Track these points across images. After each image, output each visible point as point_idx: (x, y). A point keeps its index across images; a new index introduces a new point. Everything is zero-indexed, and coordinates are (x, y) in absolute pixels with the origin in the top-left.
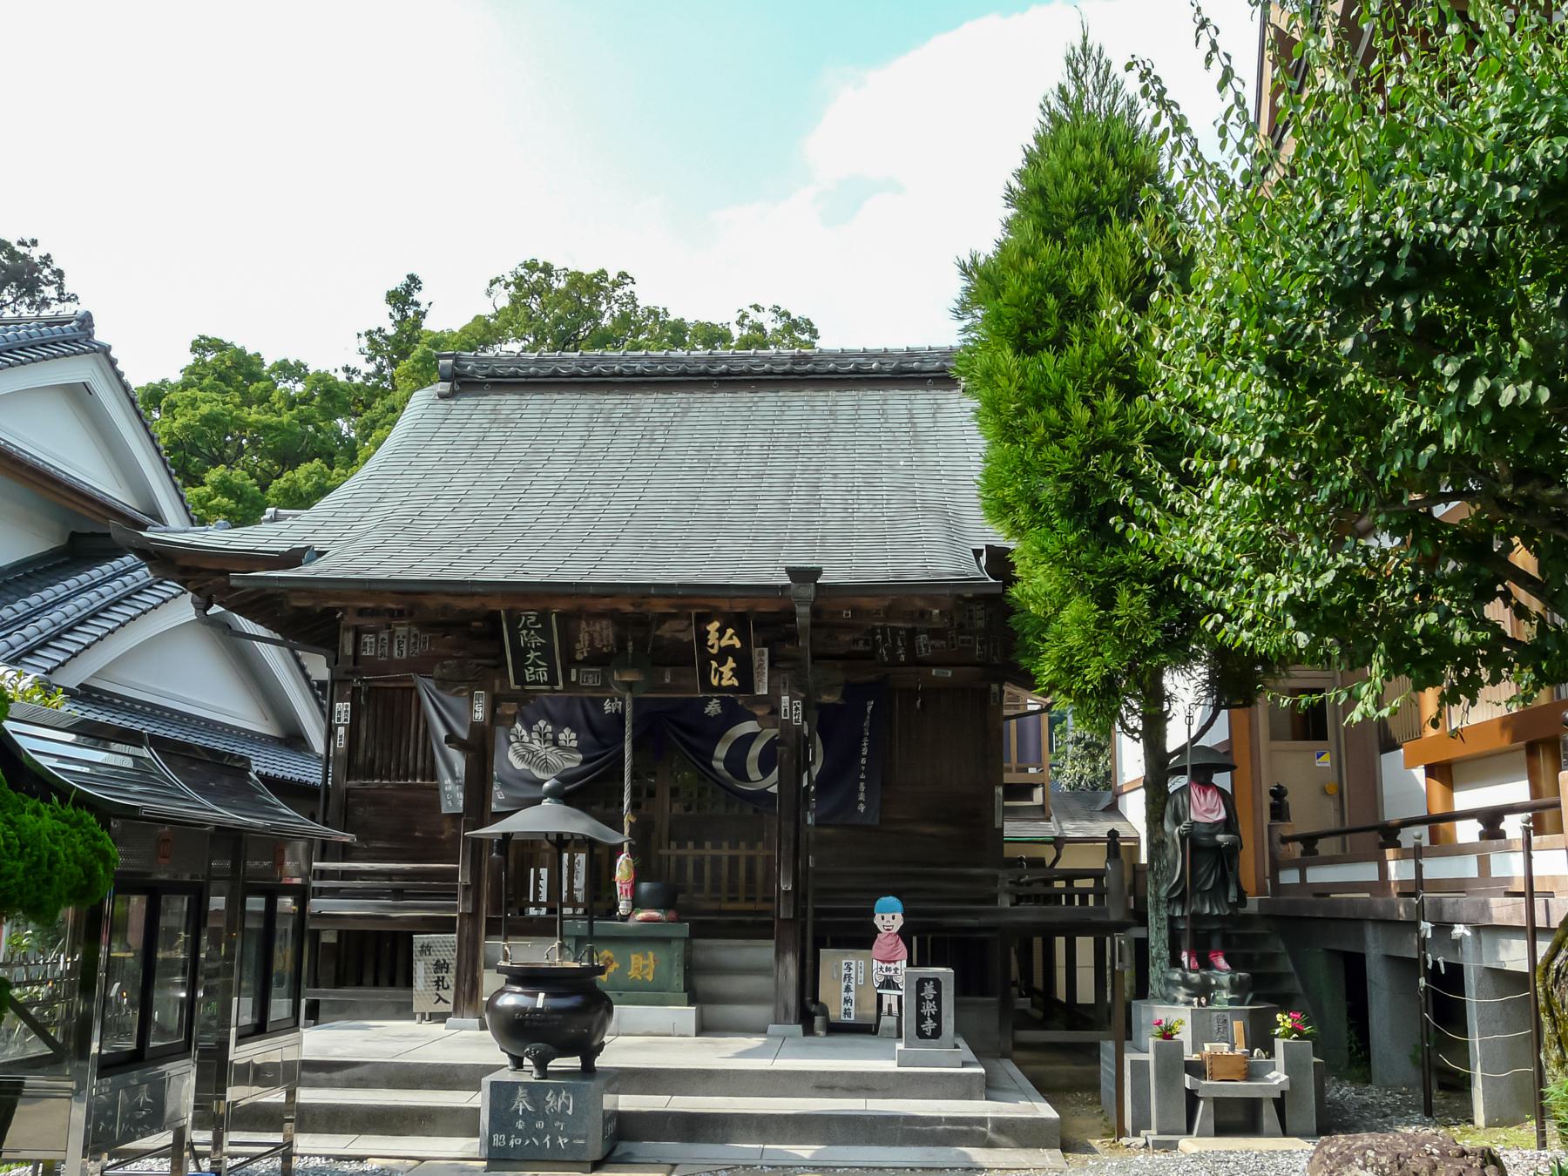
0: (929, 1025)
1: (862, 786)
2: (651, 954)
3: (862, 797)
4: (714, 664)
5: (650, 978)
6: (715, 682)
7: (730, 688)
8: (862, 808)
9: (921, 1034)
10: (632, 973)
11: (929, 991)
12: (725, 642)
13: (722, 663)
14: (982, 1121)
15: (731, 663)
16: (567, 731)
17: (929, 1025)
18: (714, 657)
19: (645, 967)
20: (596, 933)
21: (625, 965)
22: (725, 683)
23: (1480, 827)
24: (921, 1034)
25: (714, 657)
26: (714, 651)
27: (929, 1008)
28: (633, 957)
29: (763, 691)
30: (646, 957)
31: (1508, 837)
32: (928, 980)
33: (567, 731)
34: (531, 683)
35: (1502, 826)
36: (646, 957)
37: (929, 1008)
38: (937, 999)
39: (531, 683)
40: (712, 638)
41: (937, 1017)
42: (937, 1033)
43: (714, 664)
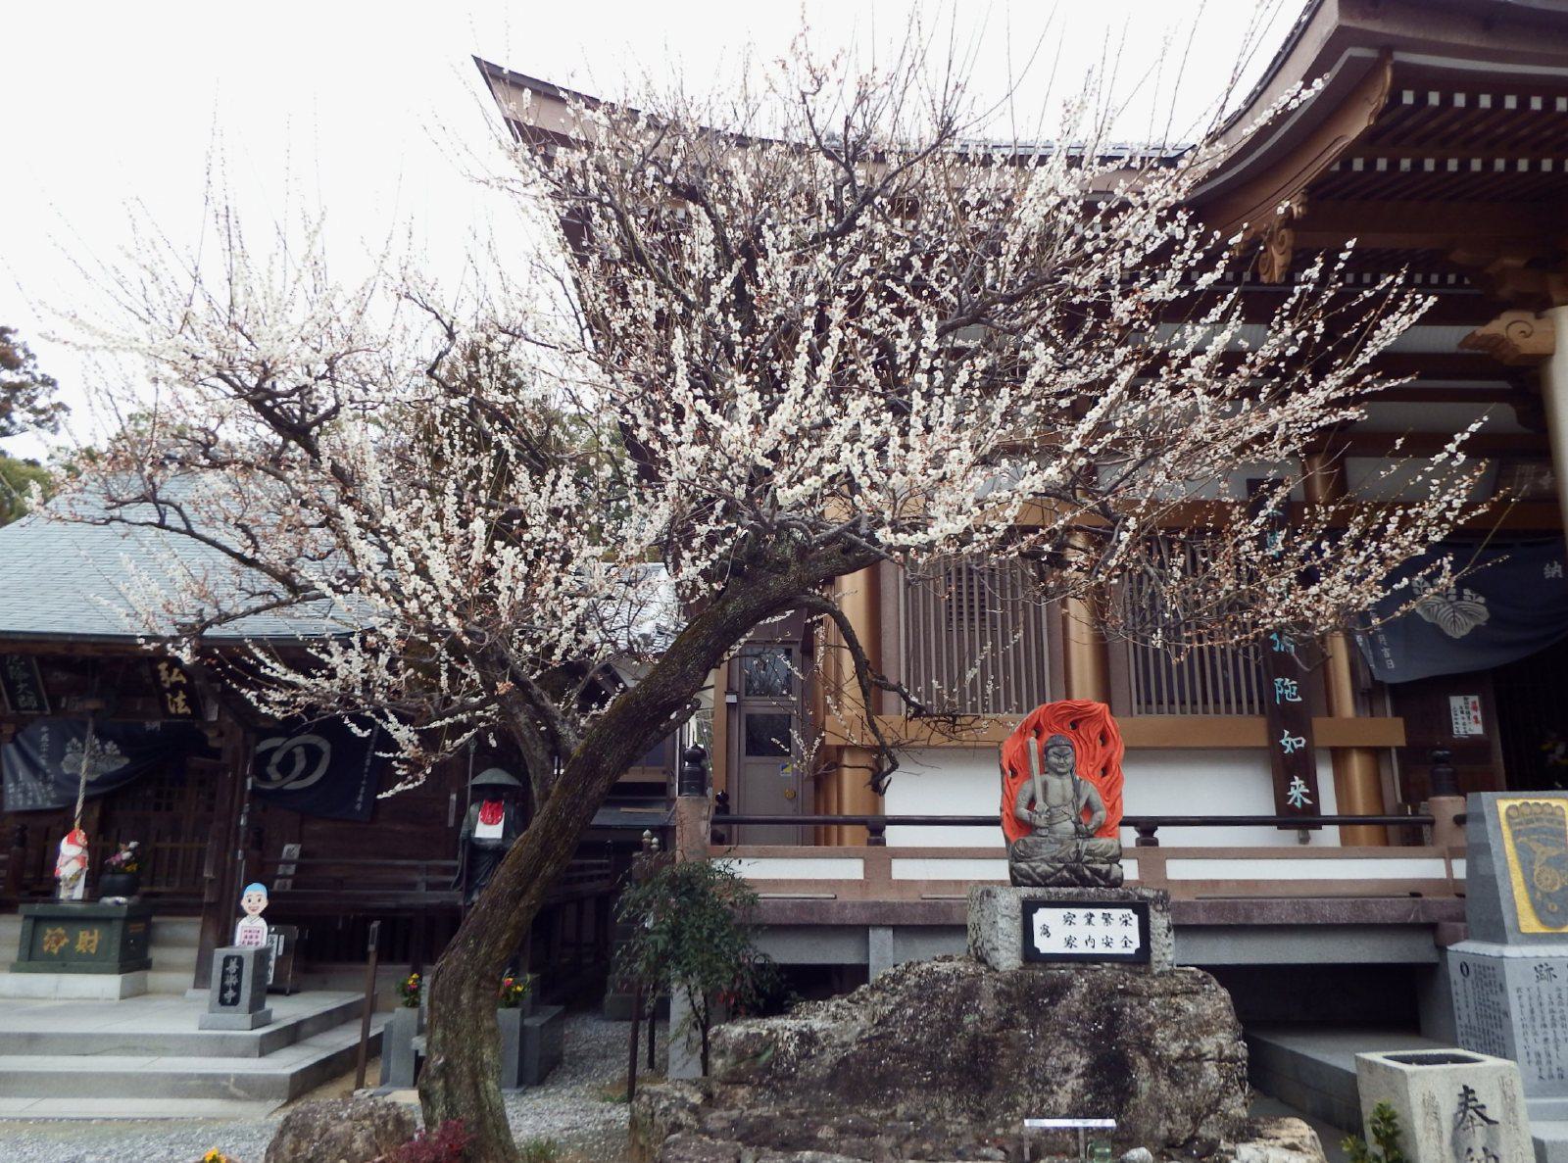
0: (230, 994)
1: (362, 791)
2: (96, 931)
3: (360, 799)
4: (169, 696)
5: (93, 951)
6: (172, 710)
7: (185, 715)
8: (359, 807)
9: (223, 1002)
10: (79, 947)
11: (233, 967)
12: (174, 678)
13: (176, 695)
14: (226, 1077)
15: (181, 696)
16: (110, 743)
17: (230, 994)
18: (168, 690)
19: (90, 942)
20: (862, 811)
21: (74, 940)
22: (181, 711)
23: (1137, 835)
24: (223, 1002)
25: (168, 690)
26: (167, 685)
27: (231, 981)
28: (81, 933)
29: (214, 718)
30: (92, 934)
31: (1161, 845)
32: (233, 957)
33: (110, 743)
34: (26, 709)
35: (1156, 835)
36: (92, 934)
37: (231, 981)
38: (239, 973)
39: (26, 709)
40: (164, 675)
41: (237, 988)
42: (235, 1001)
43: (169, 696)
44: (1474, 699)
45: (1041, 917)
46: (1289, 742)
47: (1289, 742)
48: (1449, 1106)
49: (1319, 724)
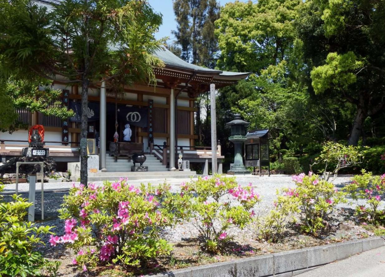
44: (93, 127)
45: (34, 151)
46: (65, 131)
47: (65, 131)
48: (75, 166)
49: (70, 129)
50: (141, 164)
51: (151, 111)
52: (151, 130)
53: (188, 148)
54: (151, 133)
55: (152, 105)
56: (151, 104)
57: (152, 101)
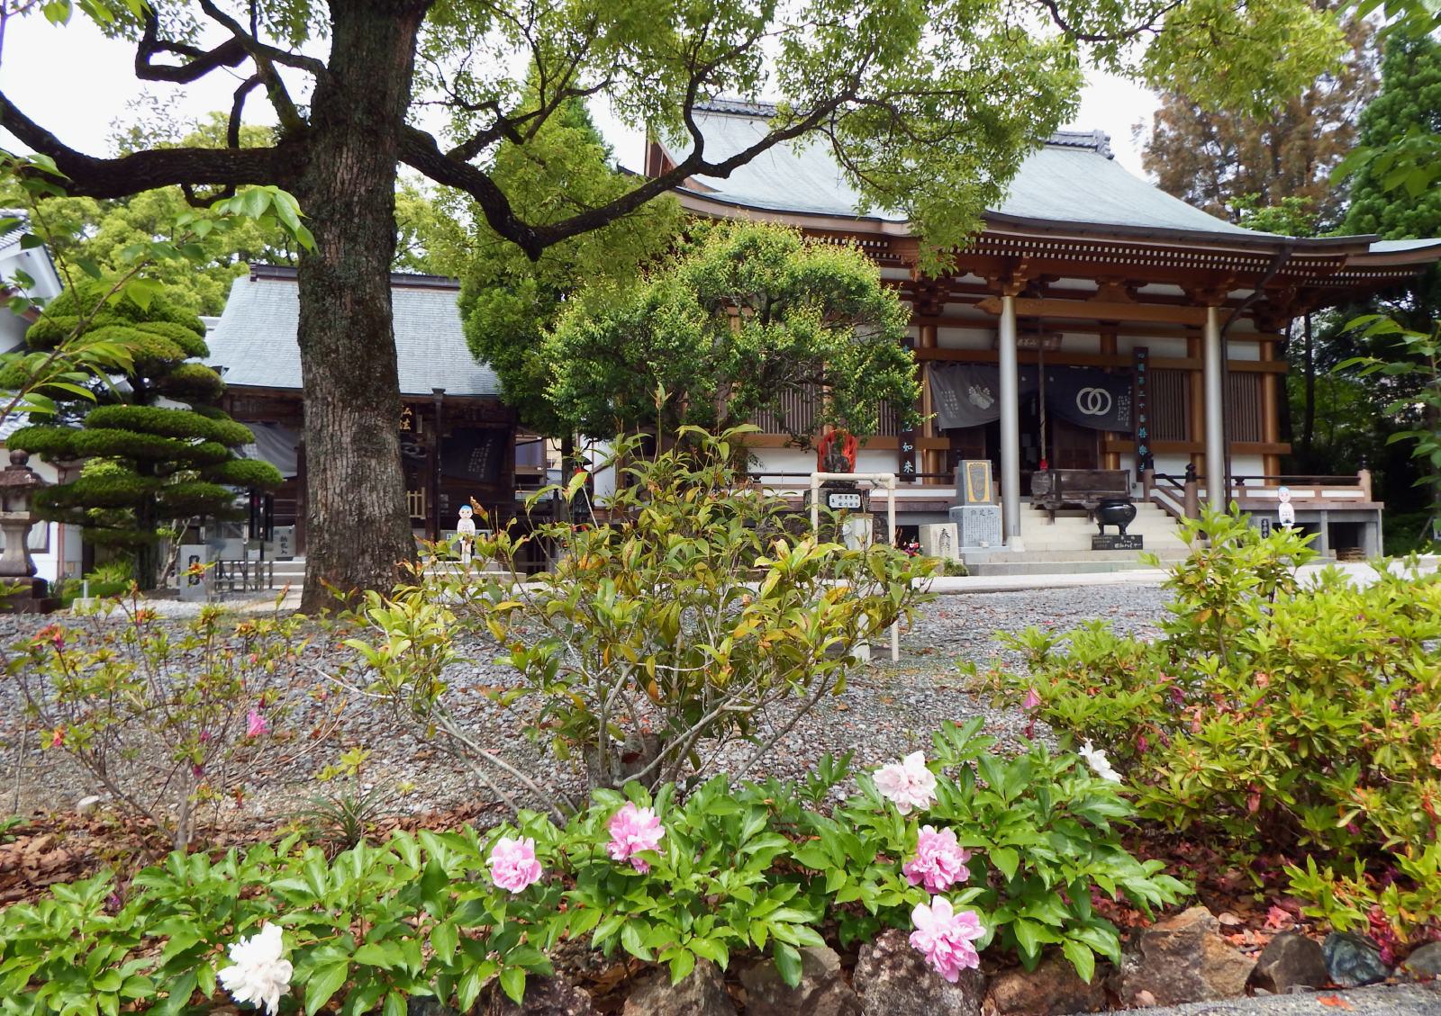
44: (519, 438)
46: (906, 447)
47: (906, 447)
50: (1122, 530)
51: (1141, 380)
52: (1142, 433)
53: (1261, 483)
54: (1144, 442)
55: (1146, 360)
56: (1141, 361)
57: (1145, 350)
